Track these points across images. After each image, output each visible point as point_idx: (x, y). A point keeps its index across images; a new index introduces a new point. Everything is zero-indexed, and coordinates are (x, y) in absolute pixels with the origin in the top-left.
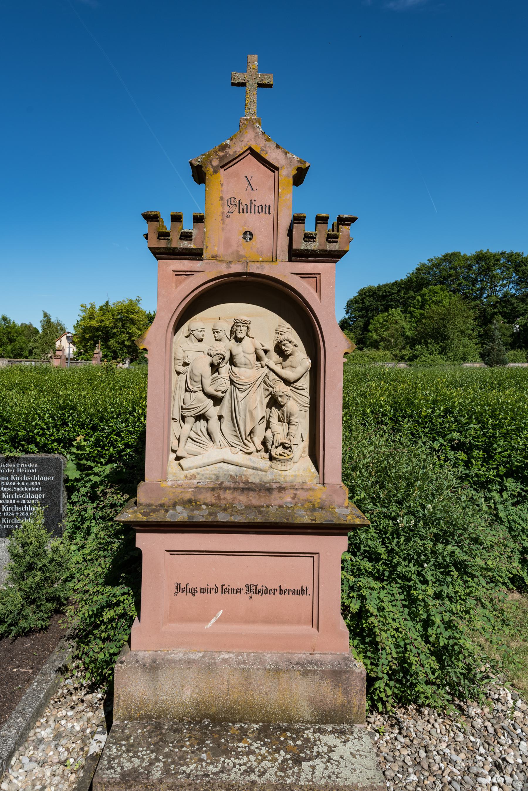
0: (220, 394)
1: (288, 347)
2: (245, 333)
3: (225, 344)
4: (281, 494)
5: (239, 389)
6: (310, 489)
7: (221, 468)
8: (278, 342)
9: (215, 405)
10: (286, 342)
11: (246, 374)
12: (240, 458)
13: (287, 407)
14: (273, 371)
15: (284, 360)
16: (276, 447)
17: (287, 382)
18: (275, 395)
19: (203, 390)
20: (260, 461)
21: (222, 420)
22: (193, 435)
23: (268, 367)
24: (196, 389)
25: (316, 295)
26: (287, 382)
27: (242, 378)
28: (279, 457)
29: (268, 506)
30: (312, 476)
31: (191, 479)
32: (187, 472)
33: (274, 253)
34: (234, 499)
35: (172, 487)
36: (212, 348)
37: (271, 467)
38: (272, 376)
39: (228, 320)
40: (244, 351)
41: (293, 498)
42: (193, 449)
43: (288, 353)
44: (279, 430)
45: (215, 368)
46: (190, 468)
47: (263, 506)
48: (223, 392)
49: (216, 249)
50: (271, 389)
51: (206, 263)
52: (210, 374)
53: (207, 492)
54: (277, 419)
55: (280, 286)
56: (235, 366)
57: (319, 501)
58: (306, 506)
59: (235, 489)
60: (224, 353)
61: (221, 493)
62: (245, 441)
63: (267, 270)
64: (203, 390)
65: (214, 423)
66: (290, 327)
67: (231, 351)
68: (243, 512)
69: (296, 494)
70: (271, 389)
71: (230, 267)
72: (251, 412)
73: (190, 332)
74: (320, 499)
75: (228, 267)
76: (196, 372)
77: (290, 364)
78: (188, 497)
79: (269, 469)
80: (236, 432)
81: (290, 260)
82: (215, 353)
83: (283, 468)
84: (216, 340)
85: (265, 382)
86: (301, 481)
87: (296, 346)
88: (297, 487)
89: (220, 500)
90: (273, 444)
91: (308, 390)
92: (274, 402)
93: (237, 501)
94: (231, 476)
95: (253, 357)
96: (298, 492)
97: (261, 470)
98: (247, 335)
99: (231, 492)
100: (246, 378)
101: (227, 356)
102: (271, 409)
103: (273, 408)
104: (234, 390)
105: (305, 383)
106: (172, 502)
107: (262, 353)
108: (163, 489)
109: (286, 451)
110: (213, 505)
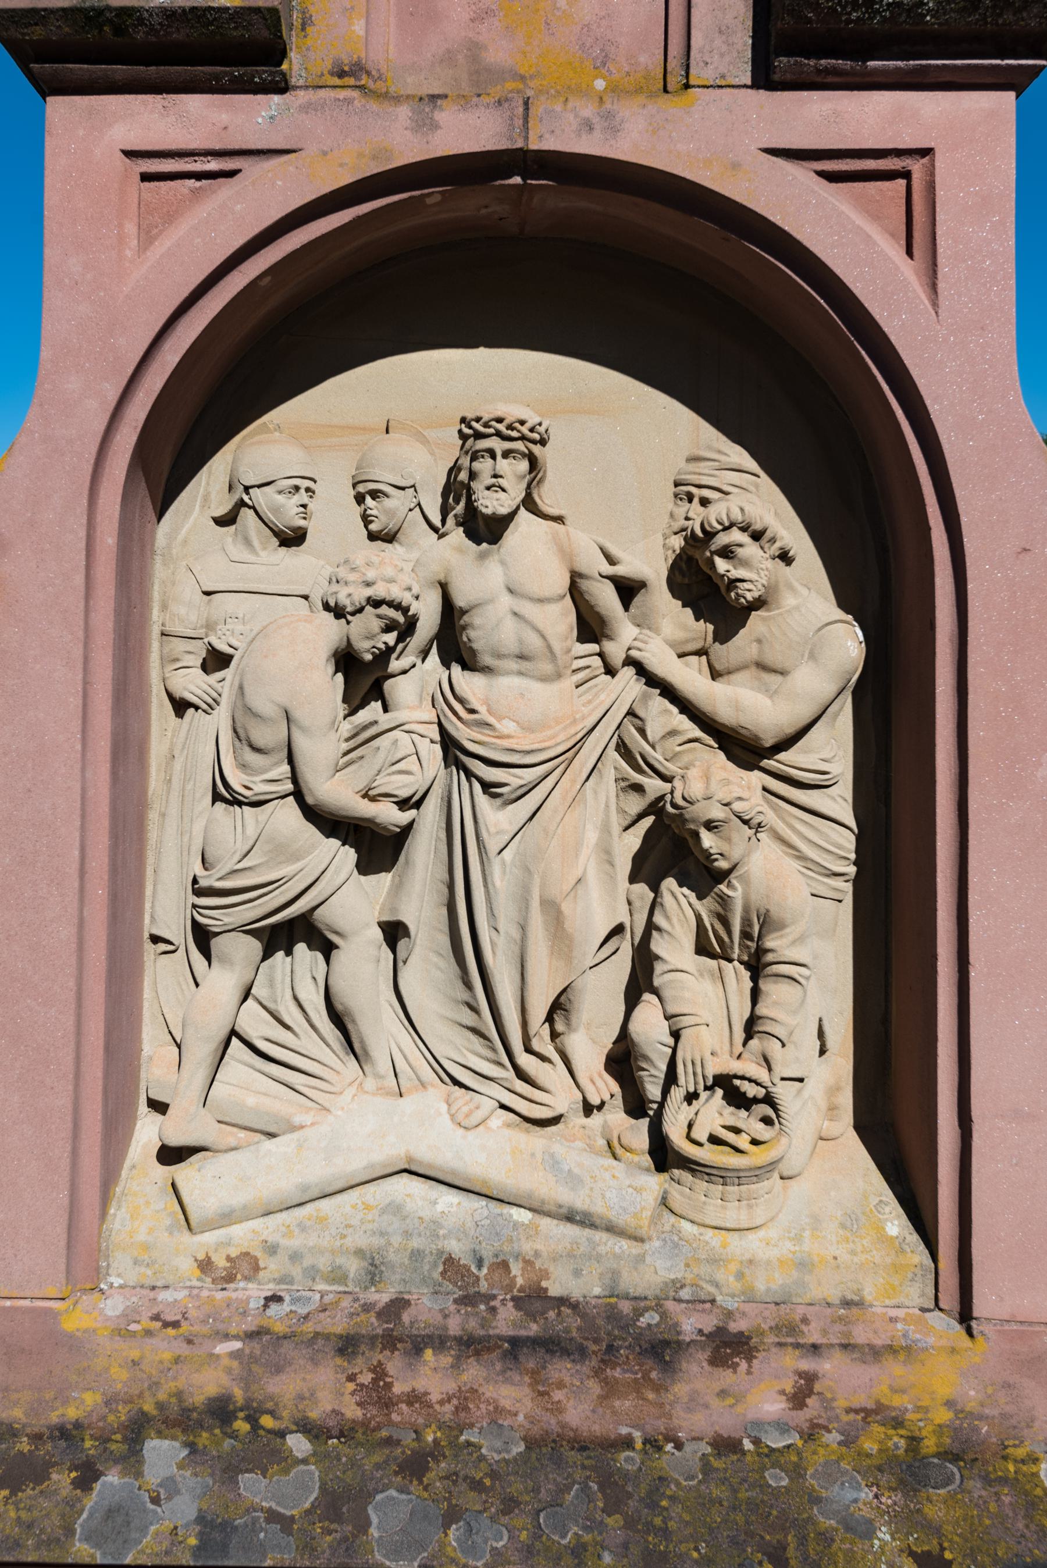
0: (389, 815)
1: (745, 563)
2: (516, 493)
3: (415, 555)
4: (726, 1377)
5: (487, 787)
6: (892, 1350)
7: (395, 1209)
8: (692, 540)
9: (364, 867)
10: (736, 536)
11: (525, 706)
12: (494, 1149)
13: (745, 880)
14: (669, 692)
15: (723, 635)
16: (691, 1097)
17: (743, 748)
18: (681, 819)
19: (298, 794)
20: (597, 1167)
21: (402, 944)
22: (254, 1023)
23: (641, 670)
24: (261, 788)
25: (908, 271)
26: (743, 748)
27: (506, 726)
28: (707, 1154)
29: (653, 1444)
30: (896, 1268)
31: (230, 1278)
32: (209, 1238)
33: (674, 63)
34: (465, 1399)
35: (121, 1333)
36: (343, 573)
37: (664, 1202)
38: (662, 716)
39: (431, 434)
40: (516, 586)
41: (798, 1399)
42: (251, 1101)
43: (749, 593)
44: (702, 994)
45: (363, 677)
46: (227, 1218)
47: (628, 1443)
48: (403, 804)
49: (359, 28)
50: (654, 786)
51: (305, 108)
52: (341, 709)
53: (315, 1362)
54: (689, 942)
55: (702, 236)
56: (469, 662)
57: (944, 1416)
58: (870, 1446)
59: (472, 1346)
60: (406, 598)
61: (394, 1364)
62: (525, 1060)
63: (639, 137)
64: (298, 794)
65: (361, 961)
66: (750, 463)
67: (444, 587)
68: (516, 1487)
69: (810, 1378)
70: (654, 786)
71: (435, 126)
72: (553, 911)
73: (239, 493)
74: (949, 1404)
75: (425, 125)
76: (262, 701)
77: (752, 652)
78: (212, 1390)
79: (655, 1220)
80: (474, 1009)
81: (764, 78)
82: (362, 594)
83: (733, 1215)
84: (372, 537)
85: (624, 749)
86: (834, 1295)
87: (785, 557)
88: (813, 1335)
89: (387, 1404)
90: (671, 1078)
91: (845, 789)
92: (672, 851)
93: (480, 1411)
94: (450, 1262)
95: (561, 620)
96: (826, 1366)
97: (611, 1229)
98: (529, 503)
99: (446, 1360)
100: (528, 728)
101: (428, 615)
102: (655, 888)
103: (669, 884)
104: (464, 793)
105: (831, 751)
106: (123, 1413)
107: (607, 598)
108: (74, 1345)
109: (740, 1117)
110: (346, 1432)
